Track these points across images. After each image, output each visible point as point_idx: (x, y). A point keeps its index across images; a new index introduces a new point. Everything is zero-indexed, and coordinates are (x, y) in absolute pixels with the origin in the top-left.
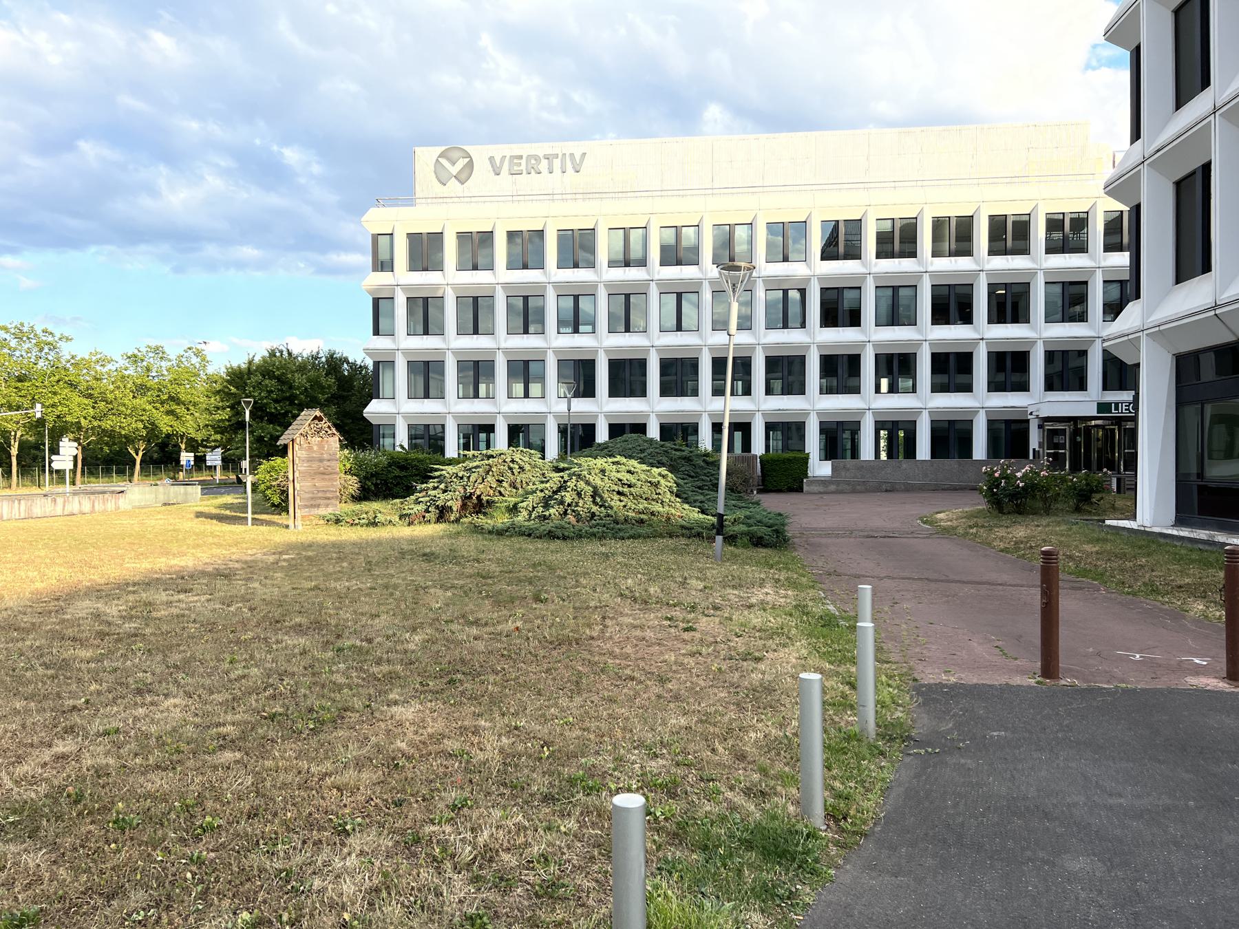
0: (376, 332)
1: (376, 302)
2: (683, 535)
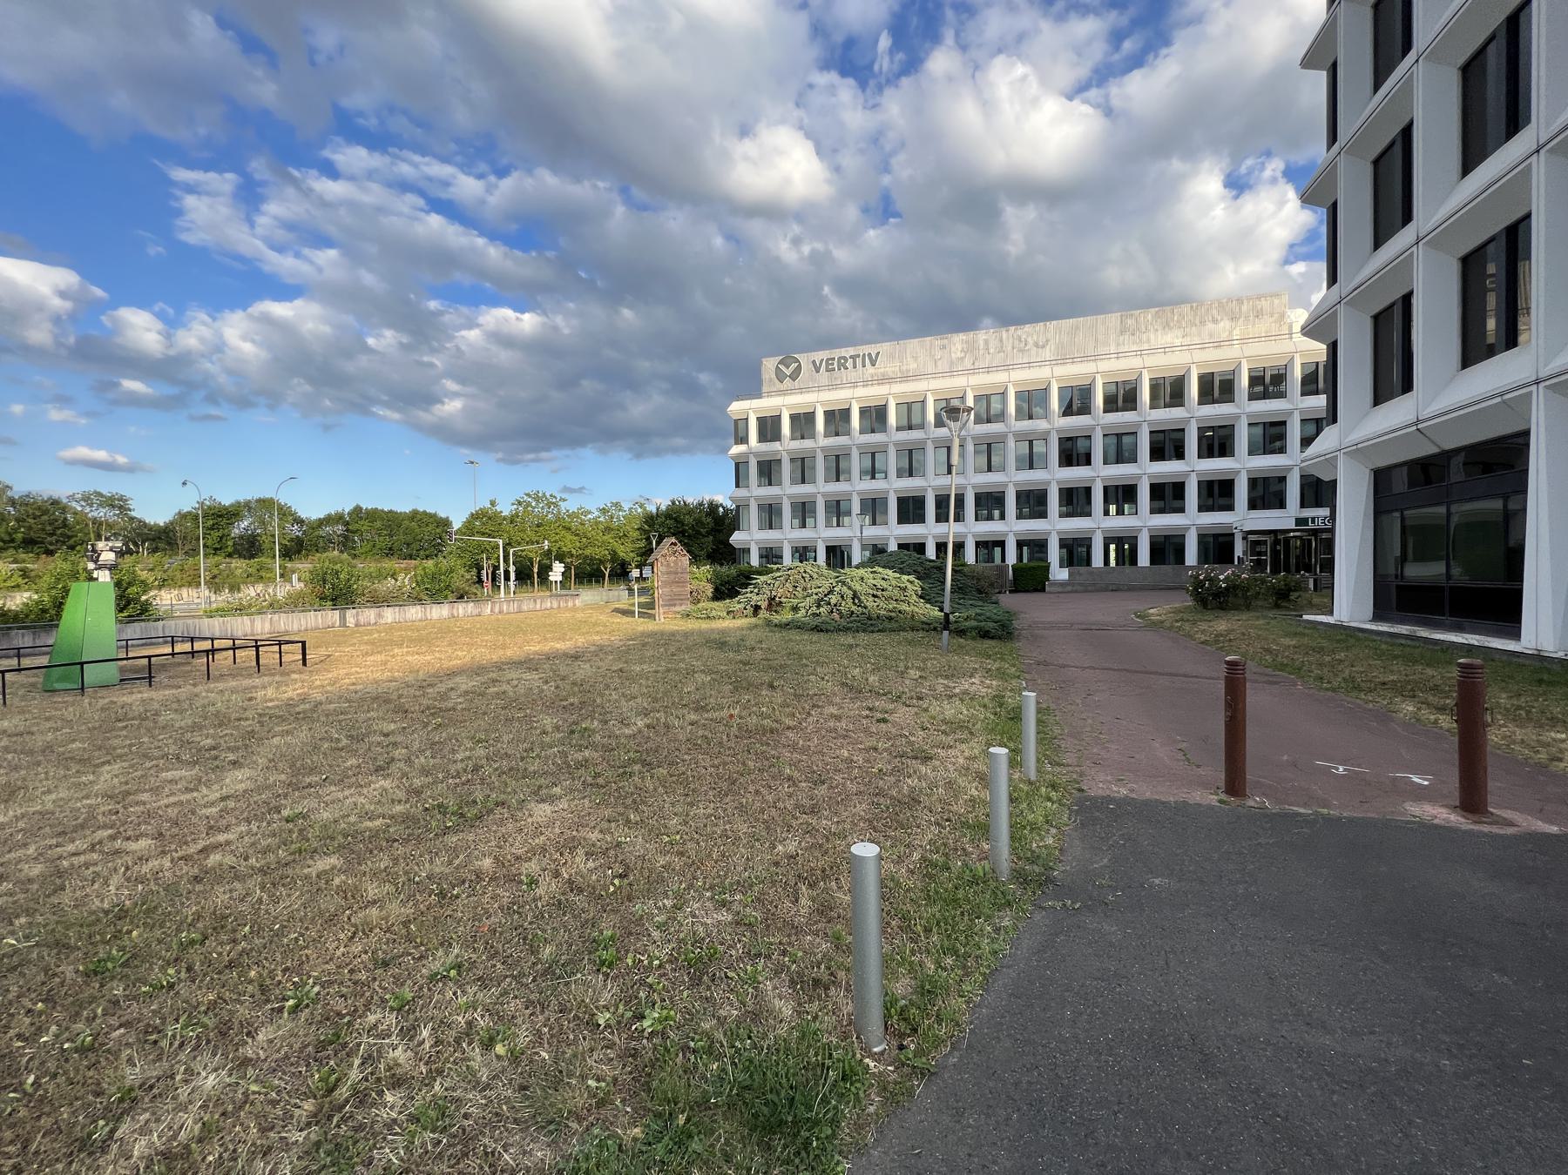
0: (737, 486)
1: (737, 465)
2: (923, 629)
